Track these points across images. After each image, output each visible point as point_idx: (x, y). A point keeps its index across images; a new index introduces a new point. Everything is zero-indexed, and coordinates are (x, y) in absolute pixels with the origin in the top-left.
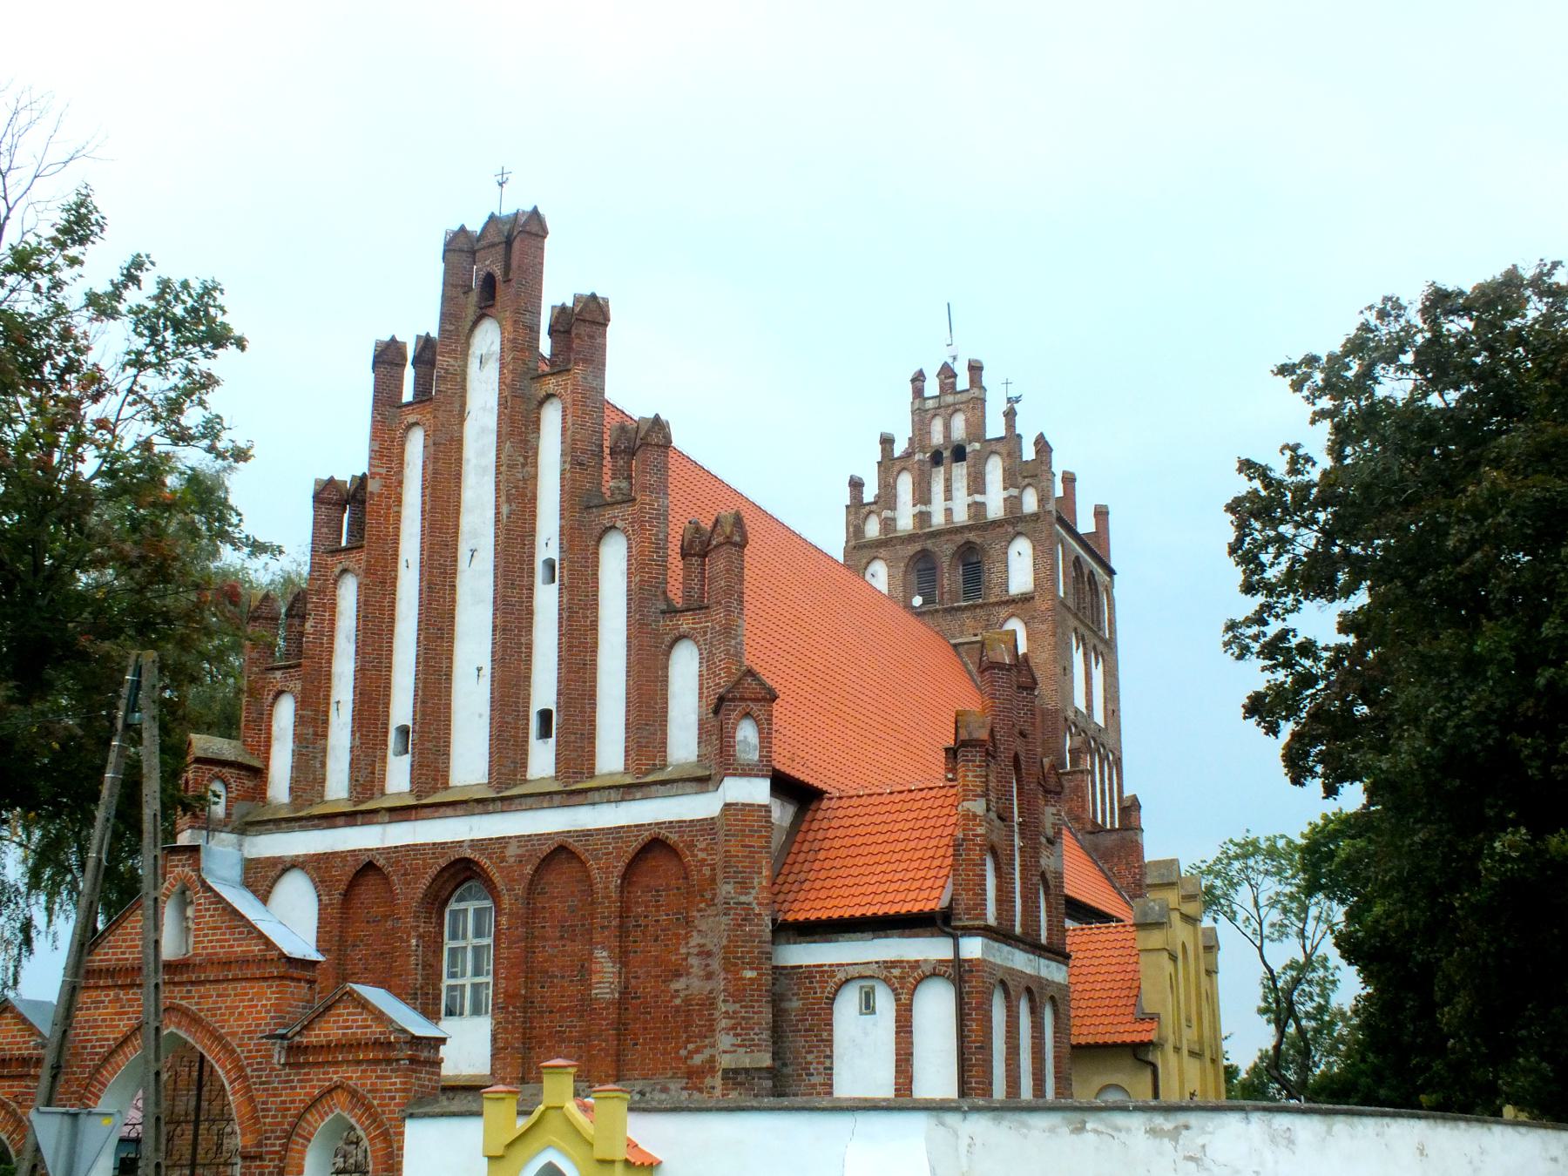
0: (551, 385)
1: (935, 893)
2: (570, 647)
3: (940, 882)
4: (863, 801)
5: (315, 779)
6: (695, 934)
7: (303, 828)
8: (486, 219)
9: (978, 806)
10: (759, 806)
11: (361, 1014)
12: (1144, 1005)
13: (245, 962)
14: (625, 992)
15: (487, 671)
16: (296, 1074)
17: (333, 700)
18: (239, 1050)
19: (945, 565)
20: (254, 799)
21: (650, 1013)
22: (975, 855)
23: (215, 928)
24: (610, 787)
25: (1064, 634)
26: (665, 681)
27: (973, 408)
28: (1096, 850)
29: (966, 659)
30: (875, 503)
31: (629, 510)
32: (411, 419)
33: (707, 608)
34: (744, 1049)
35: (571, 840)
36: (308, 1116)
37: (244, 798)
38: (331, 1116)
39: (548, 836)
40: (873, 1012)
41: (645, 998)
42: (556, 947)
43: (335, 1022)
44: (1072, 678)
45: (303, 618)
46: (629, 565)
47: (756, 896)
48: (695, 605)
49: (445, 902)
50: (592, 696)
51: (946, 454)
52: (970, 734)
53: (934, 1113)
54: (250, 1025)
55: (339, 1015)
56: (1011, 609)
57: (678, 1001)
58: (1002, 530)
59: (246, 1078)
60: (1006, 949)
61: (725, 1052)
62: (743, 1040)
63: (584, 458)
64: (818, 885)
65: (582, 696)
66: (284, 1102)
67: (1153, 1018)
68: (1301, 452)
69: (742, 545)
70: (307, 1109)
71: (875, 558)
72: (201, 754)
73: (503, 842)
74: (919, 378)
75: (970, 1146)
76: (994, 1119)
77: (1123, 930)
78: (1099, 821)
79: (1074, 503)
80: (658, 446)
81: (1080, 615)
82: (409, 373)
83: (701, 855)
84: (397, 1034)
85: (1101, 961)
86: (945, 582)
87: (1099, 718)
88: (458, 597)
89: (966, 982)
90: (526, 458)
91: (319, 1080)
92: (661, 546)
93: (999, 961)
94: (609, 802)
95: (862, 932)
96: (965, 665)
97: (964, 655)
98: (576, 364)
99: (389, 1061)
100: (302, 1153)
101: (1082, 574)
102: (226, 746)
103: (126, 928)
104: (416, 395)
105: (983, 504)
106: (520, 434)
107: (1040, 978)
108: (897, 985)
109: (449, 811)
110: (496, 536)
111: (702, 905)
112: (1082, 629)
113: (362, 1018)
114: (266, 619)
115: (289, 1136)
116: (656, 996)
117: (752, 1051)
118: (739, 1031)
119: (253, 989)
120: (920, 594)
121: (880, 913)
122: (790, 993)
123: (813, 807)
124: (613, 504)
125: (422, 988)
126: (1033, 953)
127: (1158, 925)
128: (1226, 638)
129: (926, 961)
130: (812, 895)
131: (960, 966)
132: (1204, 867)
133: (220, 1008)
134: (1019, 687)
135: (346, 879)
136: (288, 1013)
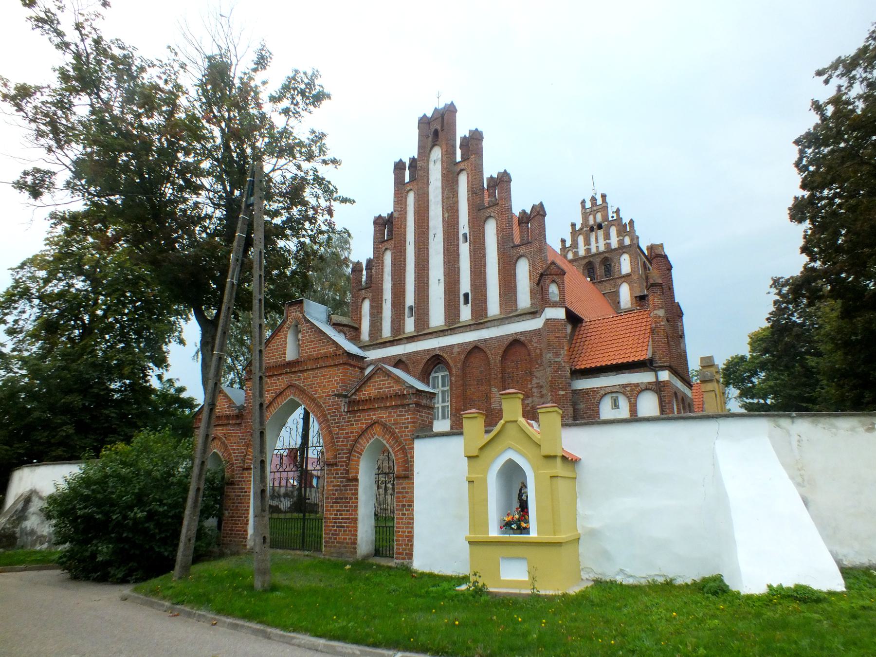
2: (475, 265)
3: (647, 339)
7: (374, 349)
11: (387, 380)
13: (326, 357)
16: (354, 417)
17: (384, 299)
18: (324, 406)
23: (311, 342)
24: (494, 320)
31: (496, 208)
32: (408, 188)
36: (360, 440)
38: (373, 440)
39: (470, 343)
43: (373, 386)
45: (371, 269)
47: (562, 357)
49: (430, 374)
50: (485, 285)
51: (595, 227)
53: (772, 419)
54: (329, 392)
55: (375, 382)
56: (623, 280)
57: (529, 408)
59: (327, 420)
63: (477, 191)
64: (587, 354)
66: (347, 433)
70: (360, 436)
72: (335, 322)
73: (452, 346)
74: (583, 202)
75: (799, 441)
76: (813, 422)
82: (407, 172)
83: (535, 345)
86: (598, 272)
91: (365, 420)
99: (403, 406)
100: (358, 461)
103: (270, 347)
104: (410, 178)
109: (430, 336)
110: (443, 227)
113: (389, 382)
115: (350, 452)
119: (329, 372)
123: (579, 325)
129: (642, 383)
130: (586, 358)
133: (314, 384)
136: (349, 384)
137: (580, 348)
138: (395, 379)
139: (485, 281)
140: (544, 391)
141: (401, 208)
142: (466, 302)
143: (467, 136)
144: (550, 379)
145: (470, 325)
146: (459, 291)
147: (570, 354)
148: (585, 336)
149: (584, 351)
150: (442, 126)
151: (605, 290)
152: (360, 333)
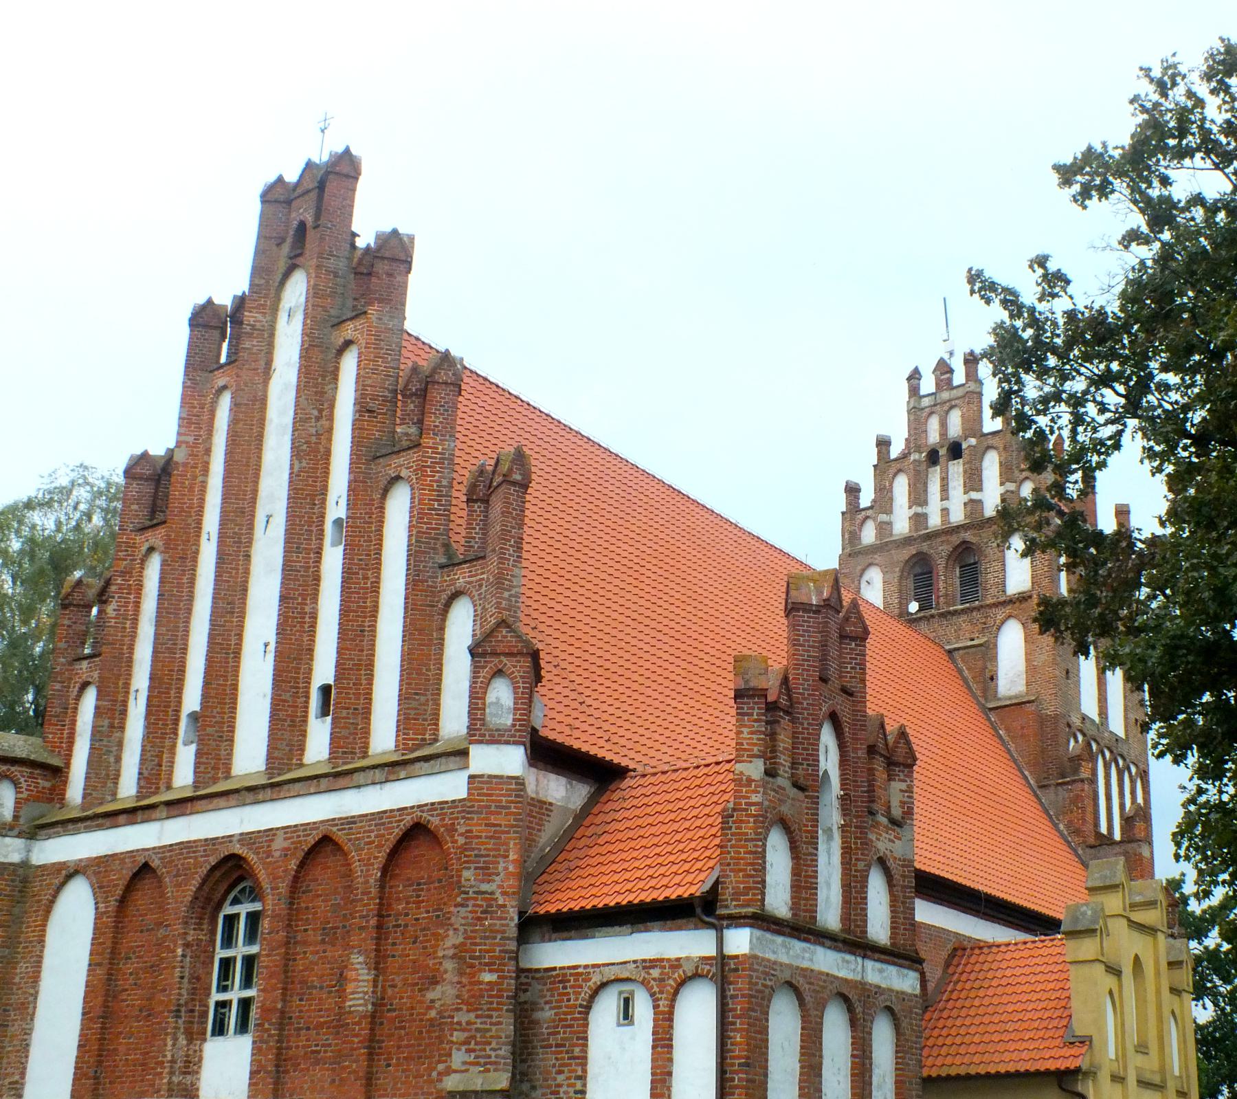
5: (108, 775)
6: (451, 933)
7: (88, 829)
8: (303, 166)
10: (509, 777)
14: (380, 1004)
15: (272, 647)
19: (941, 569)
20: (50, 800)
21: (404, 1028)
29: (961, 665)
30: (871, 508)
31: (413, 456)
35: (335, 829)
37: (37, 799)
40: (631, 1023)
42: (317, 952)
50: (370, 666)
51: (942, 452)
56: (1008, 610)
57: (433, 1014)
65: (358, 667)
67: (1086, 1041)
68: (1052, 266)
69: (524, 486)
71: (870, 565)
73: (270, 833)
74: (915, 376)
78: (1104, 830)
86: (941, 585)
88: (252, 568)
89: (731, 983)
90: (321, 411)
92: (443, 495)
95: (621, 925)
96: (960, 671)
97: (959, 661)
102: (21, 743)
105: (980, 502)
106: (316, 386)
107: (865, 984)
108: (656, 989)
109: (221, 802)
114: (78, 606)
116: (412, 1008)
117: (488, 1071)
118: (472, 1046)
120: (915, 600)
122: (542, 1001)
123: (612, 787)
125: (186, 1003)
126: (854, 954)
127: (1090, 932)
129: (688, 958)
131: (723, 965)
135: (122, 883)
141: (197, 438)
143: (372, 245)
150: (318, 216)
151: (958, 639)
152: (65, 783)
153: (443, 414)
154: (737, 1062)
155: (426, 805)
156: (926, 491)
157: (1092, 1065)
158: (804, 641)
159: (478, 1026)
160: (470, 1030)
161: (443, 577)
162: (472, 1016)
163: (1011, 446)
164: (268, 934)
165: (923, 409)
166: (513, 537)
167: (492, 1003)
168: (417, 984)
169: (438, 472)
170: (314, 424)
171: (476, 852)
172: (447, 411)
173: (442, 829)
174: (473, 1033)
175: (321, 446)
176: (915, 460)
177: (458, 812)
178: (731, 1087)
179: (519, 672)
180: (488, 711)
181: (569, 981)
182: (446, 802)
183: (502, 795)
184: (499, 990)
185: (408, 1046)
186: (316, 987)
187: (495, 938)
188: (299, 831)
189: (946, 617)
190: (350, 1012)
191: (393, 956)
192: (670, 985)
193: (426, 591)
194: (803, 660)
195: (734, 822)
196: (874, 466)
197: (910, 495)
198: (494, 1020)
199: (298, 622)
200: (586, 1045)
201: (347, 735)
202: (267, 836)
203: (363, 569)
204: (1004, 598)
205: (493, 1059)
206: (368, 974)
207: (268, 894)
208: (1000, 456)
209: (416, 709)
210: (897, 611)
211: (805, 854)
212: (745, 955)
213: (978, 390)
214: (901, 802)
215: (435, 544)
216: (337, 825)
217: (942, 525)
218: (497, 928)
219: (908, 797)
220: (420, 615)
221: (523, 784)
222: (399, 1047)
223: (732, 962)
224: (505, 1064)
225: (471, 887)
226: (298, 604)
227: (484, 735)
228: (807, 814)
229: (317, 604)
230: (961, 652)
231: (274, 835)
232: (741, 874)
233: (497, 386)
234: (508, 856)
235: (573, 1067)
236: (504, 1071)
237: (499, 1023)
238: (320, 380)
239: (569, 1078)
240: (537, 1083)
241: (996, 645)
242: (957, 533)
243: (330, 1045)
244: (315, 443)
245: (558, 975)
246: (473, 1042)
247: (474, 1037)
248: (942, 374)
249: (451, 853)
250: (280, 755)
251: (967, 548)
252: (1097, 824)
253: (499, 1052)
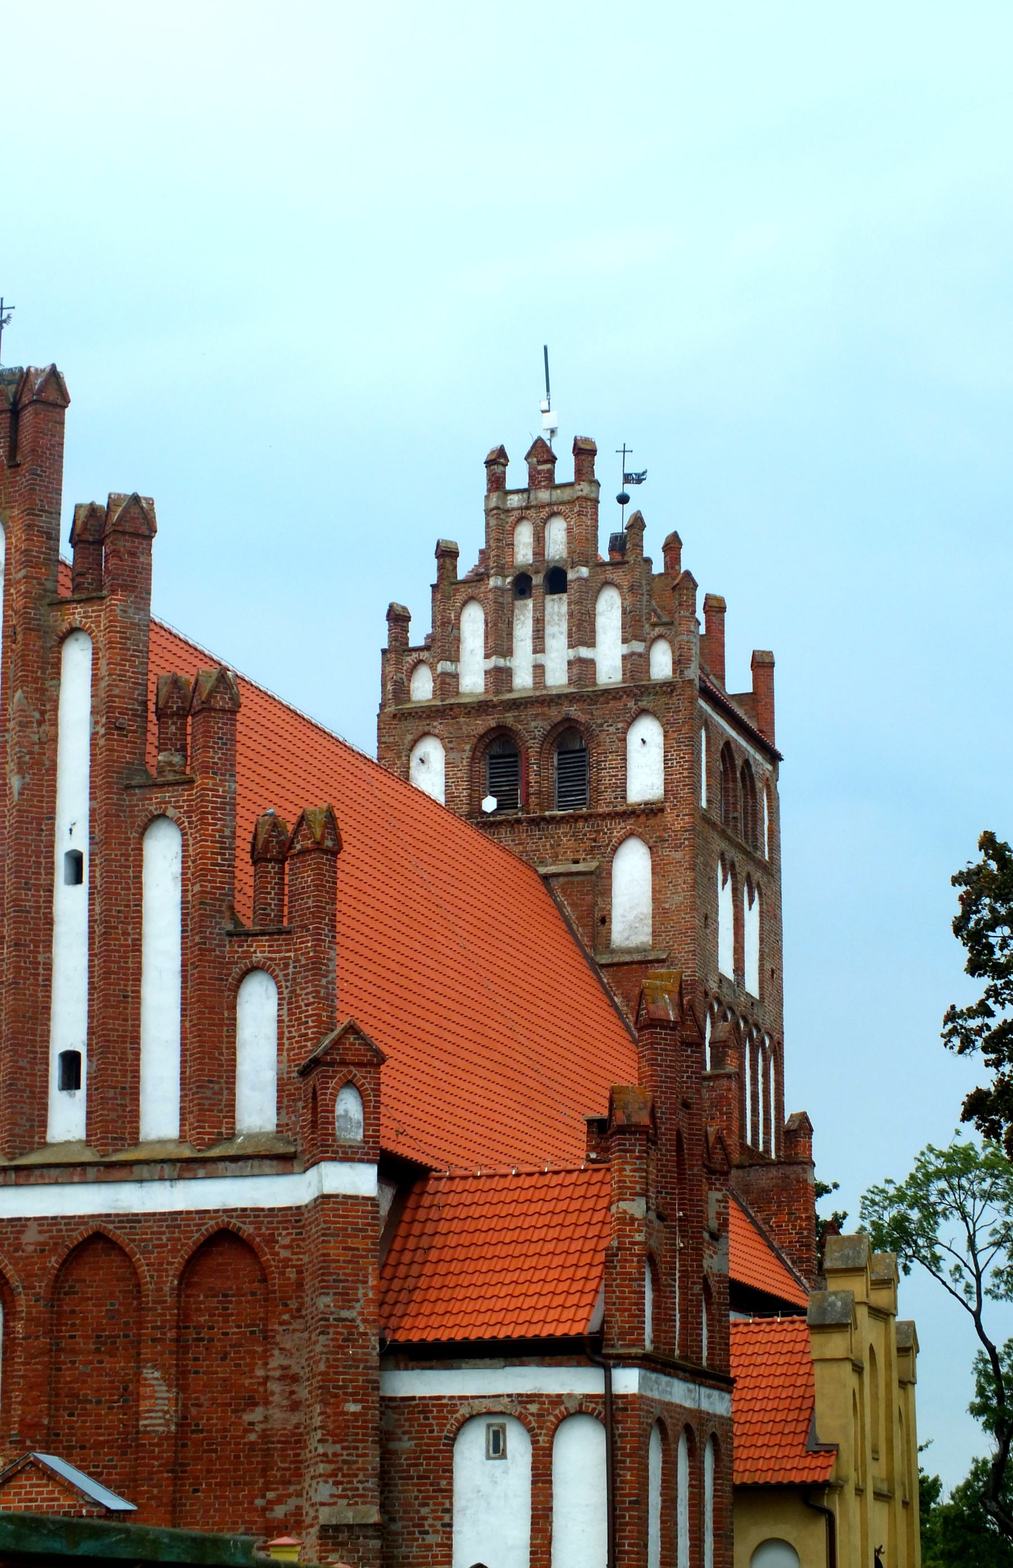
0: (77, 615)
1: (583, 1313)
3: (587, 1299)
4: (481, 1184)
9: (637, 1208)
10: (365, 1198)
11: (47, 1486)
12: (819, 1431)
21: (215, 1451)
22: (632, 1268)
24: (163, 1161)
25: (706, 864)
26: (232, 1023)
27: (580, 514)
28: (746, 1192)
29: (561, 898)
30: (426, 648)
33: (289, 933)
34: (345, 1501)
35: (111, 1226)
40: (503, 1456)
41: (210, 1431)
42: (91, 1363)
44: (716, 930)
46: (185, 868)
48: (272, 928)
50: (135, 1039)
51: (537, 580)
52: (629, 1117)
56: (629, 825)
57: (252, 1437)
58: (620, 705)
60: (664, 1379)
61: (322, 1504)
62: (344, 1490)
63: (124, 721)
64: (432, 1295)
67: (831, 1450)
69: (334, 853)
71: (426, 734)
74: (497, 460)
77: (791, 1327)
78: (749, 1142)
79: (723, 645)
80: (223, 710)
81: (729, 832)
83: (284, 1254)
84: (88, 1508)
85: (762, 1370)
86: (532, 778)
87: (752, 985)
89: (619, 1422)
90: (43, 713)
92: (226, 845)
93: (656, 1395)
94: (162, 1179)
96: (559, 907)
97: (558, 892)
98: (113, 592)
101: (733, 767)
108: (534, 1424)
111: (286, 1317)
112: (732, 854)
117: (356, 1503)
118: (340, 1478)
120: (494, 794)
121: (515, 1335)
122: (399, 1431)
123: (417, 1189)
124: (163, 785)
126: (694, 1382)
128: (945, 1031)
129: (570, 1396)
132: (892, 1191)
134: (682, 1043)
137: (415, 1270)
138: (62, 1485)
139: (137, 1027)
140: (303, 1392)
142: (70, 1081)
144: (322, 1367)
145: (83, 1165)
146: (46, 1044)
147: (384, 1284)
148: (429, 1228)
149: (423, 1283)
151: (555, 861)
153: (222, 749)
154: (627, 1499)
155: (235, 1210)
156: (510, 635)
157: (838, 1478)
158: (662, 1060)
159: (345, 1457)
160: (336, 1462)
161: (232, 946)
162: (338, 1447)
163: (640, 586)
164: (23, 1338)
165: (508, 511)
166: (327, 914)
167: (357, 1434)
168: (230, 1405)
169: (220, 819)
170: (35, 730)
171: (334, 1277)
172: (226, 744)
173: (258, 1239)
174: (340, 1465)
175: (45, 758)
176: (496, 588)
177: (278, 1222)
178: (621, 1524)
179: (369, 1083)
180: (337, 1124)
181: (432, 1412)
182: (262, 1210)
183: (358, 1217)
184: (365, 1421)
185: (219, 1471)
186: (91, 1402)
187: (358, 1367)
188: (60, 1224)
189: (538, 824)
190: (146, 1432)
191: (197, 1372)
192: (551, 1421)
193: (213, 962)
194: (661, 1081)
195: (618, 1261)
196: (432, 586)
197: (486, 637)
198: (360, 1452)
199: (31, 974)
200: (451, 1478)
201: (115, 1118)
202: (13, 1226)
203: (122, 922)
204: (624, 808)
205: (361, 1492)
206: (168, 1391)
207: (20, 1293)
208: (624, 599)
209: (210, 1099)
210: (465, 809)
211: (664, 1286)
212: (633, 1395)
213: (593, 495)
214: (718, 1213)
215: (220, 906)
216: (113, 1222)
217: (535, 689)
218: (359, 1357)
219: (724, 1207)
220: (209, 990)
221: (378, 1206)
222: (209, 1471)
223: (620, 1401)
224: (373, 1497)
225: (332, 1313)
226: (30, 952)
227: (337, 1152)
228: (666, 1244)
229: (51, 952)
230: (562, 879)
231: (25, 1226)
232: (626, 1314)
233: (196, 649)
234: (366, 1282)
235: (440, 1500)
236: (372, 1503)
237: (366, 1455)
238: (39, 674)
239: (434, 1511)
240: (397, 1516)
241: (610, 874)
242: (557, 704)
243: (115, 1467)
244: (39, 754)
245: (418, 1405)
246: (340, 1475)
247: (341, 1469)
248: (539, 463)
249: (271, 1266)
250: (21, 1132)
251: (571, 727)
252: (743, 1137)
253: (366, 1485)
